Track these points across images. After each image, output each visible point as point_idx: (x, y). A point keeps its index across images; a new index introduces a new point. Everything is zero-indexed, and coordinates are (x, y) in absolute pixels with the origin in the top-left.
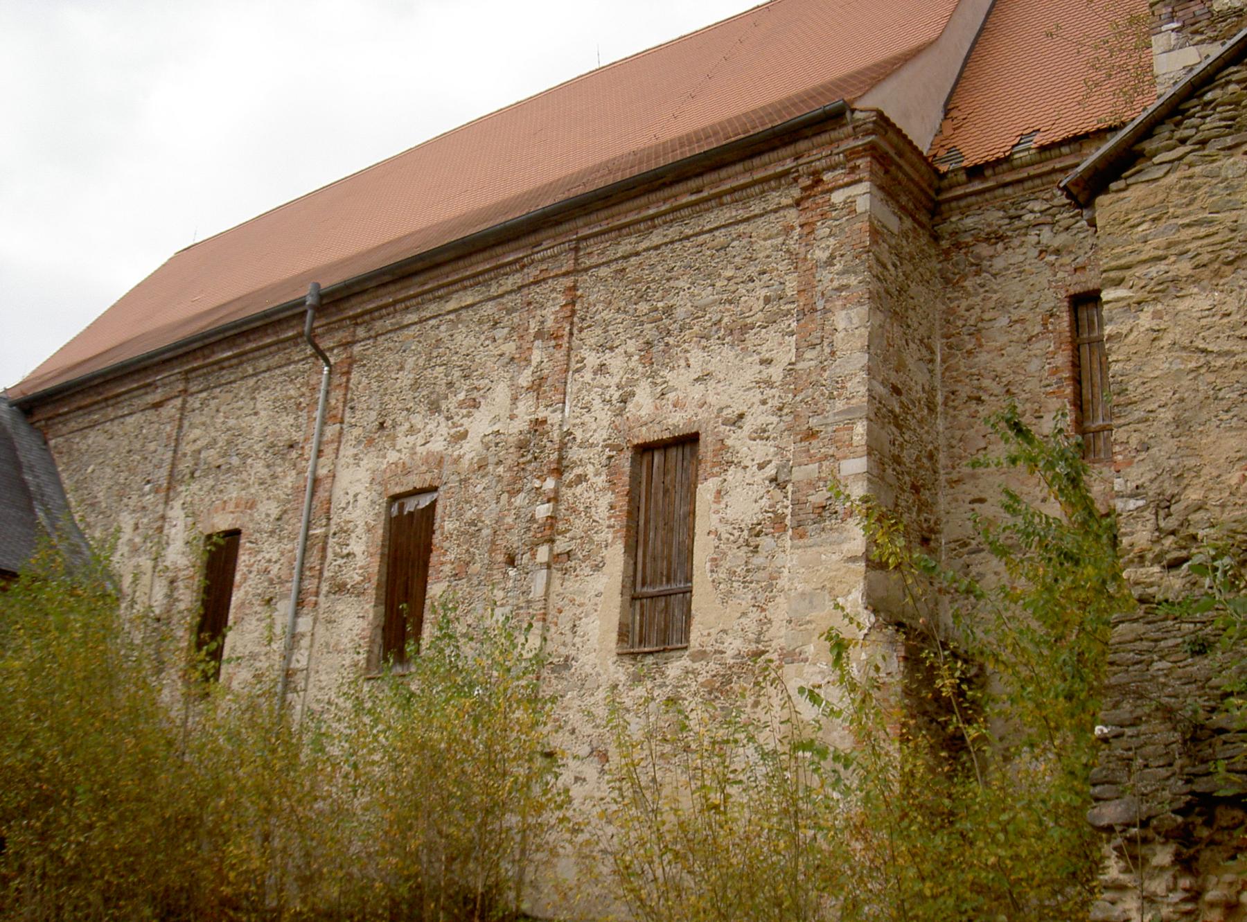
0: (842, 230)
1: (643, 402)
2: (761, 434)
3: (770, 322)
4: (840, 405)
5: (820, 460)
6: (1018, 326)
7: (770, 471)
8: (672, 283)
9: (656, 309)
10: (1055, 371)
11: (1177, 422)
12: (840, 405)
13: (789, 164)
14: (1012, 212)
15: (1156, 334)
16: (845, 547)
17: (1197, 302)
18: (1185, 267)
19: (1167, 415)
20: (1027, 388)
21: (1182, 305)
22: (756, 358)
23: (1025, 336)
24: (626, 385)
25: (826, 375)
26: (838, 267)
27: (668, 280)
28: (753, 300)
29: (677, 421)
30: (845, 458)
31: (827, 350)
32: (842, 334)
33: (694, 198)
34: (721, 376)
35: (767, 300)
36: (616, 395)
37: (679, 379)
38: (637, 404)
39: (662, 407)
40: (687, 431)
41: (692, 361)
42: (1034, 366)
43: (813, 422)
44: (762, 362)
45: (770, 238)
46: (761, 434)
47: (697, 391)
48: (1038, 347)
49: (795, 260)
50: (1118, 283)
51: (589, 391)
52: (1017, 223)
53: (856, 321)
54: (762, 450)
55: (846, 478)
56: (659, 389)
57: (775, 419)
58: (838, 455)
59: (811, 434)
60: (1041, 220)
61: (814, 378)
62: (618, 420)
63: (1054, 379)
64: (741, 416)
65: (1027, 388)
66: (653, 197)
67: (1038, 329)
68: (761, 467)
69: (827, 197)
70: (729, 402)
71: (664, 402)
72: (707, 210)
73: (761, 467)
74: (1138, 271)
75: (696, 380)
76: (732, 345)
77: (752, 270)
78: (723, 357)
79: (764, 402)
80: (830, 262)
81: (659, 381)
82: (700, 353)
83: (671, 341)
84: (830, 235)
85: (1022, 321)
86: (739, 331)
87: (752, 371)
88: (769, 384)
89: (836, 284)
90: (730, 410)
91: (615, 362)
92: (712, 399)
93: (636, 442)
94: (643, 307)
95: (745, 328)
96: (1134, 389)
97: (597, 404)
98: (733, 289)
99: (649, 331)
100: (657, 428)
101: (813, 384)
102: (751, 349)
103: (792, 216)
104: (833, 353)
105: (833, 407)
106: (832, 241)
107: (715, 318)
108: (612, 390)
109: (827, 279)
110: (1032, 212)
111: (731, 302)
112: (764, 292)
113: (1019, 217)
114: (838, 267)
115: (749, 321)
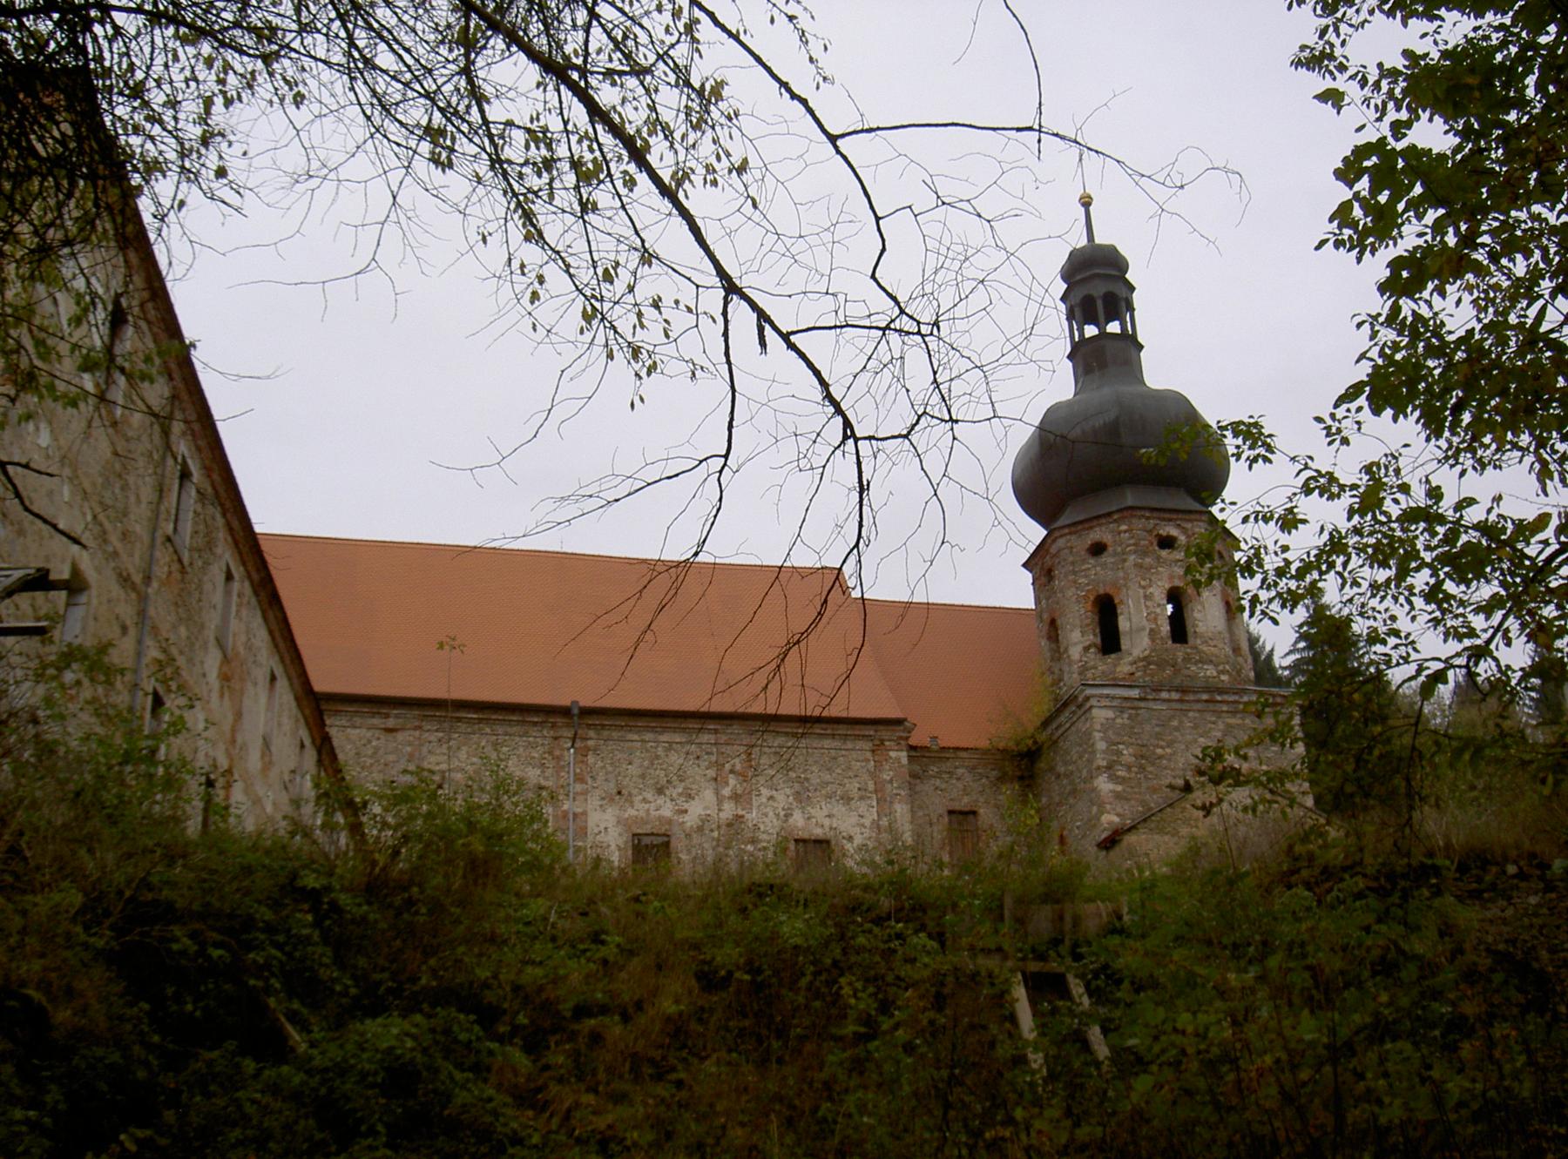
1: (798, 819)
3: (861, 798)
49: (873, 775)
78: (839, 809)
80: (891, 781)
86: (846, 799)
87: (854, 819)
91: (780, 797)
103: (869, 755)
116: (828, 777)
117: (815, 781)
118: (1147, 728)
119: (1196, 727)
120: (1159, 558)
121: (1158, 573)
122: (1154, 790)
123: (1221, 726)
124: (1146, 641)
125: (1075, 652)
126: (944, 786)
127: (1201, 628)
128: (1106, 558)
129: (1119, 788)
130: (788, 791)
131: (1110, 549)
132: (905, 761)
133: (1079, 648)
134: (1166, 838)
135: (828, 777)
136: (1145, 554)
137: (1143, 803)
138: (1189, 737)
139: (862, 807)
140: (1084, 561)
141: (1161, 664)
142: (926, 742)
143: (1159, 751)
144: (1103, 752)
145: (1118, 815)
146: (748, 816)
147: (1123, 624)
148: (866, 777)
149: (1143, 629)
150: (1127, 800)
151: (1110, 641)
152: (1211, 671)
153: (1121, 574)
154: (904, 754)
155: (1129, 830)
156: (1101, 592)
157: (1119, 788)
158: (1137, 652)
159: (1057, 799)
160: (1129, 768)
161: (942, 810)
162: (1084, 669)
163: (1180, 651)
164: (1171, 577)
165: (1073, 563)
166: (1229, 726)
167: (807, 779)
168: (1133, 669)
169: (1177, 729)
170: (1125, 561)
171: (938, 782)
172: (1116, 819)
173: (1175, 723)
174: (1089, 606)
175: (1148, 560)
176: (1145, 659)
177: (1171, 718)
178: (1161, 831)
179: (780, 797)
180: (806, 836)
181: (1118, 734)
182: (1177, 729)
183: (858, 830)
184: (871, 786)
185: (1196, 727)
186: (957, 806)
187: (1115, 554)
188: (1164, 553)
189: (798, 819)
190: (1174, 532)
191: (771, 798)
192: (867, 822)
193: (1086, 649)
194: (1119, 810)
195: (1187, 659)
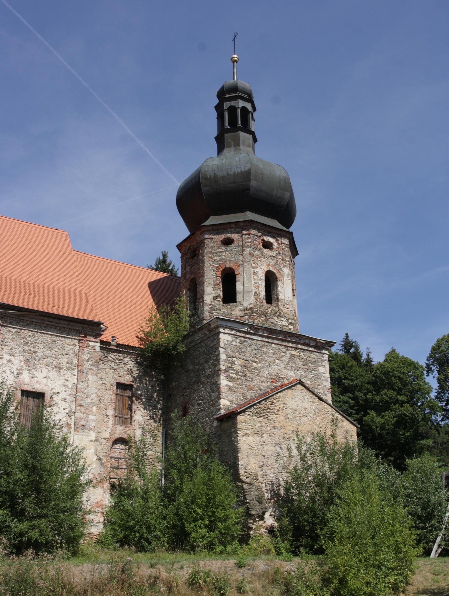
0: (92, 353)
1: (25, 377)
2: (65, 400)
3: (67, 369)
4: (89, 400)
5: (83, 413)
6: (104, 385)
7: (67, 411)
8: (36, 344)
9: (31, 350)
10: (111, 400)
11: (247, 456)
12: (89, 400)
13: (80, 329)
14: (106, 355)
15: (245, 441)
16: (90, 438)
17: (251, 438)
18: (249, 432)
19: (246, 454)
20: (105, 401)
21: (249, 438)
22: (63, 378)
23: (105, 388)
24: (20, 370)
25: (86, 391)
26: (90, 363)
27: (35, 343)
28: (64, 361)
29: (37, 387)
30: (90, 415)
31: (86, 385)
32: (91, 382)
33: (50, 323)
34: (52, 379)
35: (68, 363)
36: (16, 372)
37: (39, 375)
38: (23, 377)
39: (32, 381)
40: (41, 391)
41: (43, 371)
42: (107, 396)
43: (82, 402)
44: (65, 380)
45: (69, 345)
46: (65, 400)
47: (45, 381)
48: (108, 392)
49: (78, 356)
50: (240, 431)
51: (5, 367)
52: (106, 358)
53: (95, 380)
54: (65, 405)
55: (90, 420)
56: (32, 375)
57: (69, 397)
58: (88, 413)
59: (81, 406)
60: (112, 360)
61: (83, 390)
62: (16, 380)
63: (111, 402)
64: (58, 393)
65: (105, 401)
66: (37, 317)
67: (109, 388)
68: (64, 409)
69: (88, 342)
70: (55, 388)
71: (33, 380)
72: (50, 328)
73: (64, 409)
74: (244, 430)
75: (44, 377)
76: (56, 371)
77: (64, 352)
78: (53, 374)
79: (66, 391)
80: (88, 360)
81: (31, 373)
82: (46, 370)
83: (36, 362)
84: (88, 353)
85: (105, 384)
86: (59, 368)
87: (62, 382)
88: (67, 386)
89: (89, 367)
90: (55, 390)
91: (16, 361)
92: (49, 384)
93: (23, 389)
94: (26, 348)
95: (61, 368)
96: (242, 449)
97: (8, 372)
98: (57, 355)
99: (28, 356)
100: (31, 387)
101: (83, 392)
102: (62, 374)
103: (76, 342)
104: (88, 386)
105: (87, 400)
106: (89, 355)
107: (52, 361)
108: (14, 369)
109: (87, 365)
110: (110, 357)
111: (56, 358)
112: (67, 360)
113: (107, 357)
114: (90, 363)
115: (62, 366)
116: (48, 353)
117: (40, 354)
118: (249, 350)
119: (275, 353)
120: (262, 253)
121: (261, 261)
122: (251, 388)
123: (288, 355)
124: (253, 299)
125: (208, 299)
126: (116, 367)
127: (281, 297)
128: (232, 247)
129: (231, 384)
130: (22, 358)
131: (236, 243)
132: (98, 349)
133: (211, 297)
134: (261, 419)
135: (48, 353)
136: (256, 249)
137: (244, 395)
138: (271, 359)
139: (68, 375)
140: (219, 248)
141: (260, 314)
142: (109, 339)
143: (254, 365)
144: (225, 361)
145: (229, 401)
146: (199, 469)
147: (239, 287)
148: (73, 355)
149: (251, 292)
150: (235, 392)
151: (230, 295)
152: (285, 323)
153: (241, 258)
154: (98, 344)
155: (240, 412)
156: (228, 266)
157: (231, 384)
158: (246, 304)
159: (185, 384)
160: (237, 372)
161: (113, 381)
162: (213, 309)
163: (270, 309)
164: (268, 265)
165: (212, 247)
166: (292, 356)
167: (35, 352)
168: (242, 314)
169: (265, 353)
170: (243, 251)
171: (113, 364)
172: (228, 403)
173: (264, 349)
174: (219, 274)
175: (257, 253)
176: (250, 309)
177: (262, 347)
178: (258, 415)
179: (16, 361)
180: (29, 389)
181: (233, 351)
182: (265, 353)
183: (63, 388)
184: (75, 362)
185: (275, 353)
186: (122, 381)
187: (238, 246)
188: (265, 251)
189: (25, 377)
190: (272, 240)
191: (10, 361)
192: (70, 384)
193: (215, 298)
194: (230, 398)
195: (273, 313)
